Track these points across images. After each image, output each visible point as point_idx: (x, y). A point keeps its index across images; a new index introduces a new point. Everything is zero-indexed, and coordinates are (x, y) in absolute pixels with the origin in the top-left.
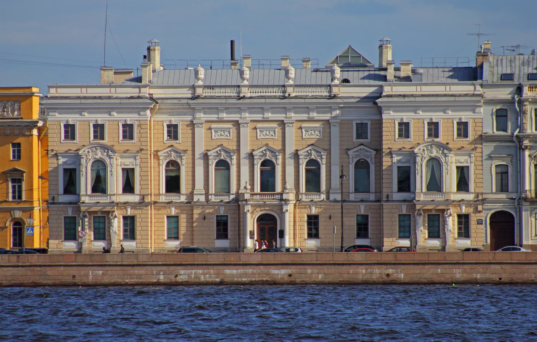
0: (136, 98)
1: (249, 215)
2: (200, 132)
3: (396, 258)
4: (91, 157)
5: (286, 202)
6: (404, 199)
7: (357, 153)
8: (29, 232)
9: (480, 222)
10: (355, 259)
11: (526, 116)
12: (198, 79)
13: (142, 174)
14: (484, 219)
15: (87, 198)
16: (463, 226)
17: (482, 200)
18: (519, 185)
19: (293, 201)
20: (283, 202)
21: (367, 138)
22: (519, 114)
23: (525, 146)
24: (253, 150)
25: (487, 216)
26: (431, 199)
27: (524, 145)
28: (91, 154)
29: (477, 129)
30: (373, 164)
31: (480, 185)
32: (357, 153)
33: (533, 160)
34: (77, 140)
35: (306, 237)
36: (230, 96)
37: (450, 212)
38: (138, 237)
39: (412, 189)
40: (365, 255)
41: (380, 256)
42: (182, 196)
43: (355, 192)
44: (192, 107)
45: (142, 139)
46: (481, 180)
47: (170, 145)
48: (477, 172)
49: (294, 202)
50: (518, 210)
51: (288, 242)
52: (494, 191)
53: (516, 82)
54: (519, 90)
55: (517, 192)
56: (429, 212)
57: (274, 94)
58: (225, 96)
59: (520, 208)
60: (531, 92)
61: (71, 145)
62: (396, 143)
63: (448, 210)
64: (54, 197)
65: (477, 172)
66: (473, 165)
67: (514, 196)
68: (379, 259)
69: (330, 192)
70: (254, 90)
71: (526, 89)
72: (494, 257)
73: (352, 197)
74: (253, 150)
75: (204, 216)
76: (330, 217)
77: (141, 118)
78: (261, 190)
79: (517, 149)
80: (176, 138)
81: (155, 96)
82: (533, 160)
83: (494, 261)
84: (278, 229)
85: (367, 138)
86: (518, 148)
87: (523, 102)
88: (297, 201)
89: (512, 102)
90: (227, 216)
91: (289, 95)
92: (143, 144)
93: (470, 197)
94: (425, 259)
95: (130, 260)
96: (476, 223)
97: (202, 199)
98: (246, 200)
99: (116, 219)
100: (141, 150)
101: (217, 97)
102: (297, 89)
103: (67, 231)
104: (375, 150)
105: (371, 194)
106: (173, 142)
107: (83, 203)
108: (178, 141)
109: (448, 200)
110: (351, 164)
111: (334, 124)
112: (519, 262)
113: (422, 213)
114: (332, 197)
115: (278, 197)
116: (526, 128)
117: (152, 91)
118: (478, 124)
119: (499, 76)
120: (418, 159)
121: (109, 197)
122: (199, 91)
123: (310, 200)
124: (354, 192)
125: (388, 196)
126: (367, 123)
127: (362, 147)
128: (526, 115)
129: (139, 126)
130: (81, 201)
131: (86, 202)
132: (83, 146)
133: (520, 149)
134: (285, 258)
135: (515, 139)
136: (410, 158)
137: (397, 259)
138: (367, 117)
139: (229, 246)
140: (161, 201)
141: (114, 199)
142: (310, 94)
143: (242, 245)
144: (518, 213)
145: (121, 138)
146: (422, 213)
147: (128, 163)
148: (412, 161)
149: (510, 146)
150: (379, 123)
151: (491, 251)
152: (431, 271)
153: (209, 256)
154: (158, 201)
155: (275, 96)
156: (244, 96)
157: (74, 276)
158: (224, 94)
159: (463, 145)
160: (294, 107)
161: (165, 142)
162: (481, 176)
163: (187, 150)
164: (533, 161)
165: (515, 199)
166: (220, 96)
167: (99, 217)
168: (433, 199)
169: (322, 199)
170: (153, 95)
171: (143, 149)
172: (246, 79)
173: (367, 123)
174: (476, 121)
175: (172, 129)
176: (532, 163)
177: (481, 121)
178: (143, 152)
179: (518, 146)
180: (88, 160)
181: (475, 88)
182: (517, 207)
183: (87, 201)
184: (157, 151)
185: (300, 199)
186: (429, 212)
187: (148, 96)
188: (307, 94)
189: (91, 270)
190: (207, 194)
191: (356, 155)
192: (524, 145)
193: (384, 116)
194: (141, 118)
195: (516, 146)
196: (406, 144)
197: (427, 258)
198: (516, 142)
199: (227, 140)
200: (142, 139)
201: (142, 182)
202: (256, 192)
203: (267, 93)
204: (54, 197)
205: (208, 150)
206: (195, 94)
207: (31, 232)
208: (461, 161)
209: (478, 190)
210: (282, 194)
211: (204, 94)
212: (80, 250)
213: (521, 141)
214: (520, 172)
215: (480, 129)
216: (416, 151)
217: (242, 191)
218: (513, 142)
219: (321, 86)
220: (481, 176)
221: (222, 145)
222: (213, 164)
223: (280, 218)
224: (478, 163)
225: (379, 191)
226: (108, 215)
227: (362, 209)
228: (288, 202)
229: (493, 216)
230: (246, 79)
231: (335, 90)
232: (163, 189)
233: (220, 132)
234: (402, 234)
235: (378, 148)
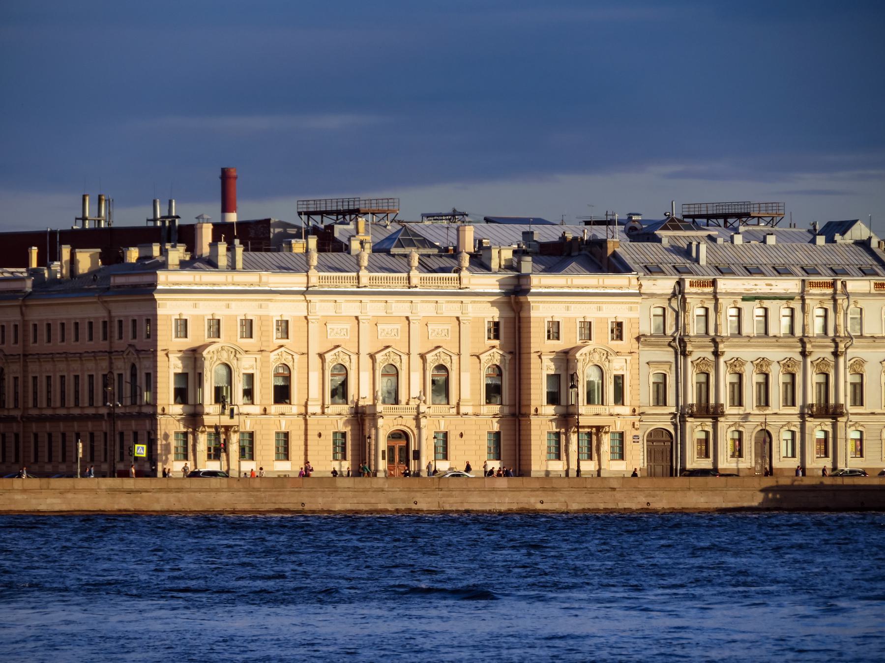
67: (673, 410)
84: (412, 448)
165: (675, 415)
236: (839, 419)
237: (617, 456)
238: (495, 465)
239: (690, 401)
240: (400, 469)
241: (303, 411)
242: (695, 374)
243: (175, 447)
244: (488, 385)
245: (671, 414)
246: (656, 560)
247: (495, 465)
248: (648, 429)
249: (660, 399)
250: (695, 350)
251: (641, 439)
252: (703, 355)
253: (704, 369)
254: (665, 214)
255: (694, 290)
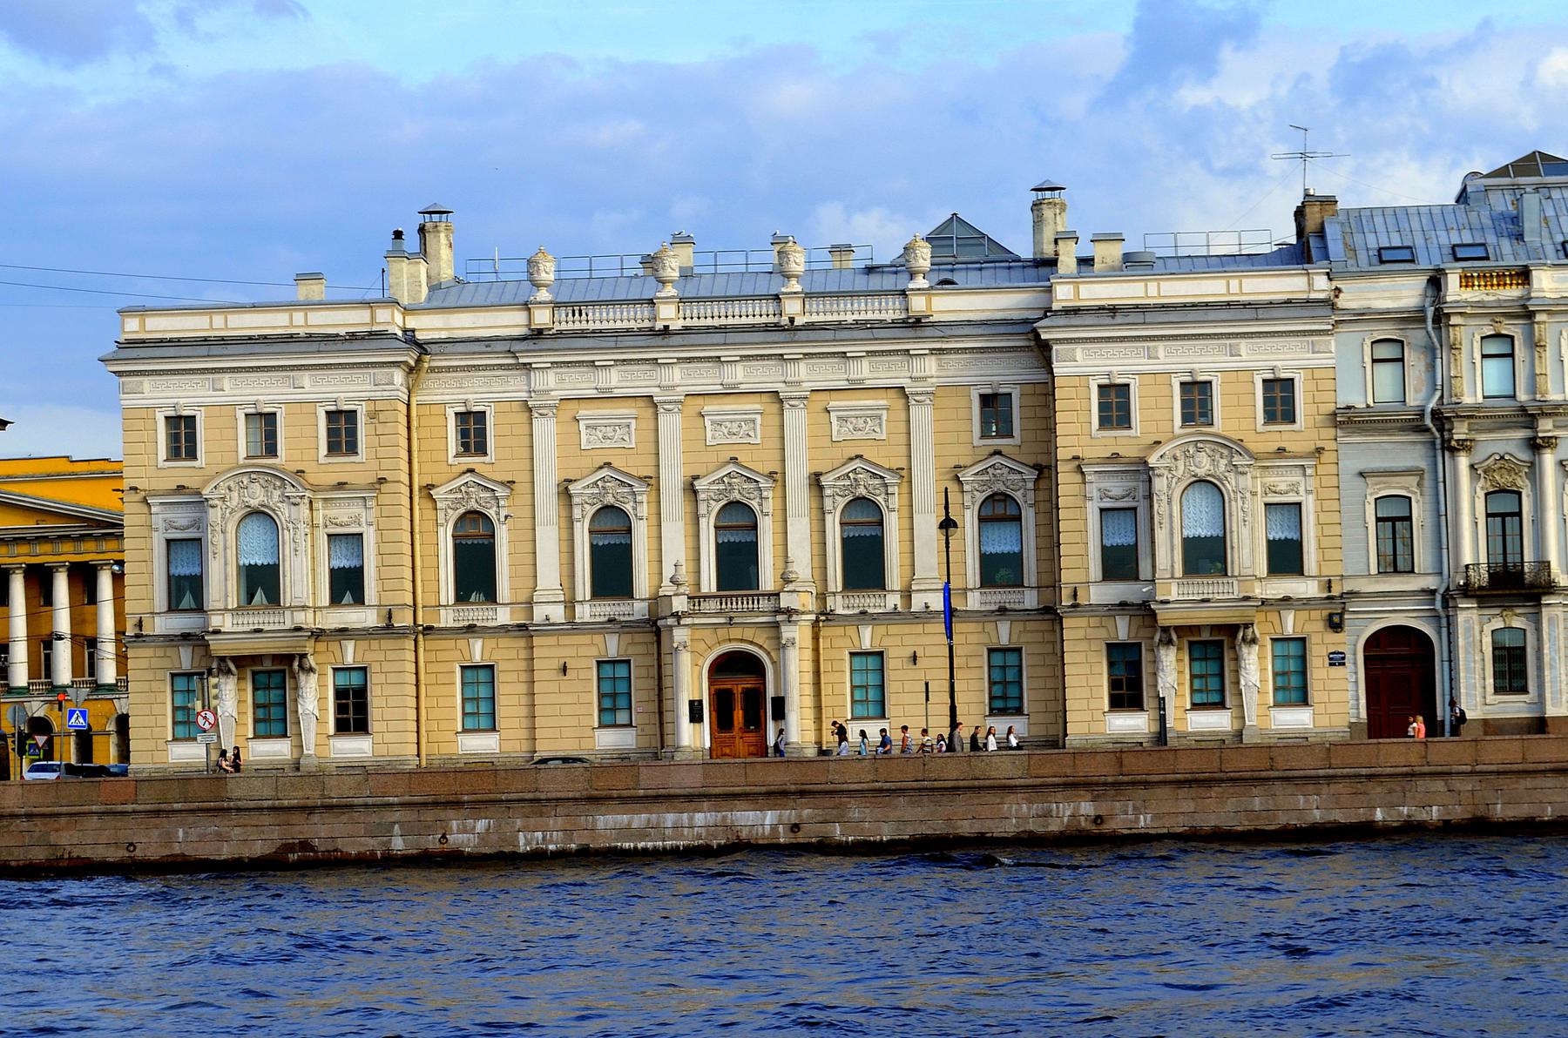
0: (363, 338)
1: (685, 659)
2: (546, 430)
3: (1121, 765)
4: (1181, 472)
5: (790, 616)
6: (1123, 599)
7: (985, 478)
8: (73, 720)
9: (1337, 660)
10: (994, 774)
11: (1458, 357)
12: (537, 285)
13: (386, 548)
14: (1346, 649)
15: (228, 617)
16: (350, 702)
17: (1341, 597)
18: (1445, 551)
19: (810, 612)
20: (779, 618)
21: (1012, 436)
22: (1439, 351)
23: (1458, 441)
24: (696, 478)
25: (1353, 641)
26: (466, 623)
27: (1455, 437)
28: (1181, 464)
29: (1320, 397)
30: (1030, 506)
31: (1337, 554)
32: (985, 478)
33: (1482, 480)
34: (201, 461)
35: (1106, 706)
36: (628, 330)
37: (1253, 632)
38: (375, 724)
39: (1144, 570)
40: (1025, 759)
41: (1071, 763)
42: (500, 609)
43: (982, 586)
44: (521, 361)
45: (382, 452)
46: (1337, 542)
47: (465, 468)
48: (1324, 518)
49: (813, 617)
50: (1444, 621)
51: (799, 730)
52: (1374, 570)
53: (1423, 263)
54: (1436, 282)
55: (1441, 574)
56: (255, 664)
57: (751, 320)
58: (616, 331)
59: (1448, 617)
60: (1469, 289)
61: (182, 473)
62: (1094, 442)
63: (1246, 626)
64: (140, 621)
65: (1324, 518)
66: (372, 529)
67: (1430, 582)
68: (1069, 771)
69: (914, 588)
70: (695, 309)
71: (1453, 282)
72: (1425, 757)
73: (974, 601)
74: (696, 478)
75: (562, 662)
76: (914, 658)
77: (378, 394)
78: (719, 588)
79: (1435, 449)
80: (481, 449)
81: (420, 336)
82: (1482, 480)
83: (1426, 769)
84: (770, 692)
85: (1012, 436)
86: (1438, 447)
87: (1448, 316)
88: (822, 614)
89: (1414, 318)
90: (1019, 650)
91: (792, 320)
92: (386, 464)
93: (1304, 588)
94: (1205, 766)
95: (301, 794)
96: (1327, 662)
97: (558, 614)
98: (677, 616)
99: (313, 678)
100: (382, 481)
101: (594, 332)
102: (814, 305)
103: (1279, 679)
104: (1034, 467)
105: (1027, 592)
106: (472, 461)
107: (217, 632)
108: (487, 459)
109: (1247, 598)
110: (704, 516)
111: (792, 403)
112: (1502, 768)
113: (1174, 637)
114: (918, 603)
115: (765, 604)
116: (1543, 389)
117: (412, 322)
118: (1323, 385)
119: (1373, 253)
120: (1160, 484)
121: (287, 613)
122: (792, 307)
123: (856, 611)
124: (978, 585)
125: (140, 625)
126: (1010, 394)
127: (997, 459)
128: (1456, 352)
129: (373, 415)
130: (211, 629)
131: (223, 630)
132: (1155, 443)
133: (1443, 449)
134: (778, 777)
135: (1428, 422)
136: (1135, 484)
137: (1125, 770)
138: (1007, 375)
139: (1229, 729)
140: (442, 625)
141: (306, 619)
142: (850, 318)
143: (669, 740)
144: (1444, 630)
145: (323, 449)
146: (1174, 637)
147: (1283, 487)
148: (1141, 493)
149: (1414, 443)
150: (1045, 394)
151: (1370, 738)
152: (1231, 804)
153: (542, 774)
154: (435, 625)
155: (754, 326)
156: (666, 327)
157: (131, 844)
158: (611, 325)
159: (1282, 445)
160: (805, 354)
161: (450, 462)
162: (1337, 530)
163: (514, 482)
164: (1482, 482)
165: (1433, 592)
166: (601, 331)
167: (269, 673)
168: (1206, 596)
169: (890, 607)
170: (417, 333)
171: (1323, 449)
172: (918, 272)
173: (1010, 394)
174: (1317, 374)
175: (343, 425)
176: (1478, 489)
177: (1330, 374)
178: (384, 487)
179: (1438, 442)
180: (1174, 480)
181: (1310, 284)
182: (1442, 614)
183: (227, 627)
184: (430, 487)
185: (828, 609)
186: (1193, 635)
187: (400, 333)
188: (842, 317)
189: (182, 825)
190: (570, 604)
191: (984, 483)
192: (1455, 437)
193: (1059, 368)
194: (378, 394)
195: (1433, 443)
196: (1125, 442)
197: (1216, 764)
198: (1434, 430)
199: (623, 451)
200: (382, 452)
201: (386, 572)
202: (705, 590)
203: (744, 317)
204: (140, 621)
205: (570, 481)
206: (530, 324)
207: (81, 720)
208: (1278, 489)
209: (1331, 570)
210: (778, 595)
211: (557, 327)
212: (1161, 736)
213: (1447, 427)
214: (1446, 515)
215: (1329, 396)
216: (1153, 461)
217: (667, 589)
218: (1428, 430)
219: (760, 298)
220: (1337, 530)
221: (734, 460)
222: (835, 508)
223: (773, 663)
224: (1325, 494)
225: (1051, 582)
226: (1234, 636)
227: (1004, 633)
228: (794, 618)
229: (1374, 642)
230: (918, 272)
231: (918, 304)
232: (447, 589)
233: (854, 421)
234: (608, 718)
235: (1042, 460)
236: (1545, 600)
237: (1294, 695)
238: (1418, 726)
239: (1467, 559)
240: (741, 742)
241: (523, 597)
242: (1481, 494)
243: (691, 703)
244: (333, 572)
245: (1423, 591)
246: (771, 869)
247: (1418, 726)
248: (1362, 631)
249: (1395, 562)
250: (1480, 437)
251: (1349, 657)
252: (1501, 448)
253: (1504, 480)
254: (1045, 196)
255: (1470, 295)
